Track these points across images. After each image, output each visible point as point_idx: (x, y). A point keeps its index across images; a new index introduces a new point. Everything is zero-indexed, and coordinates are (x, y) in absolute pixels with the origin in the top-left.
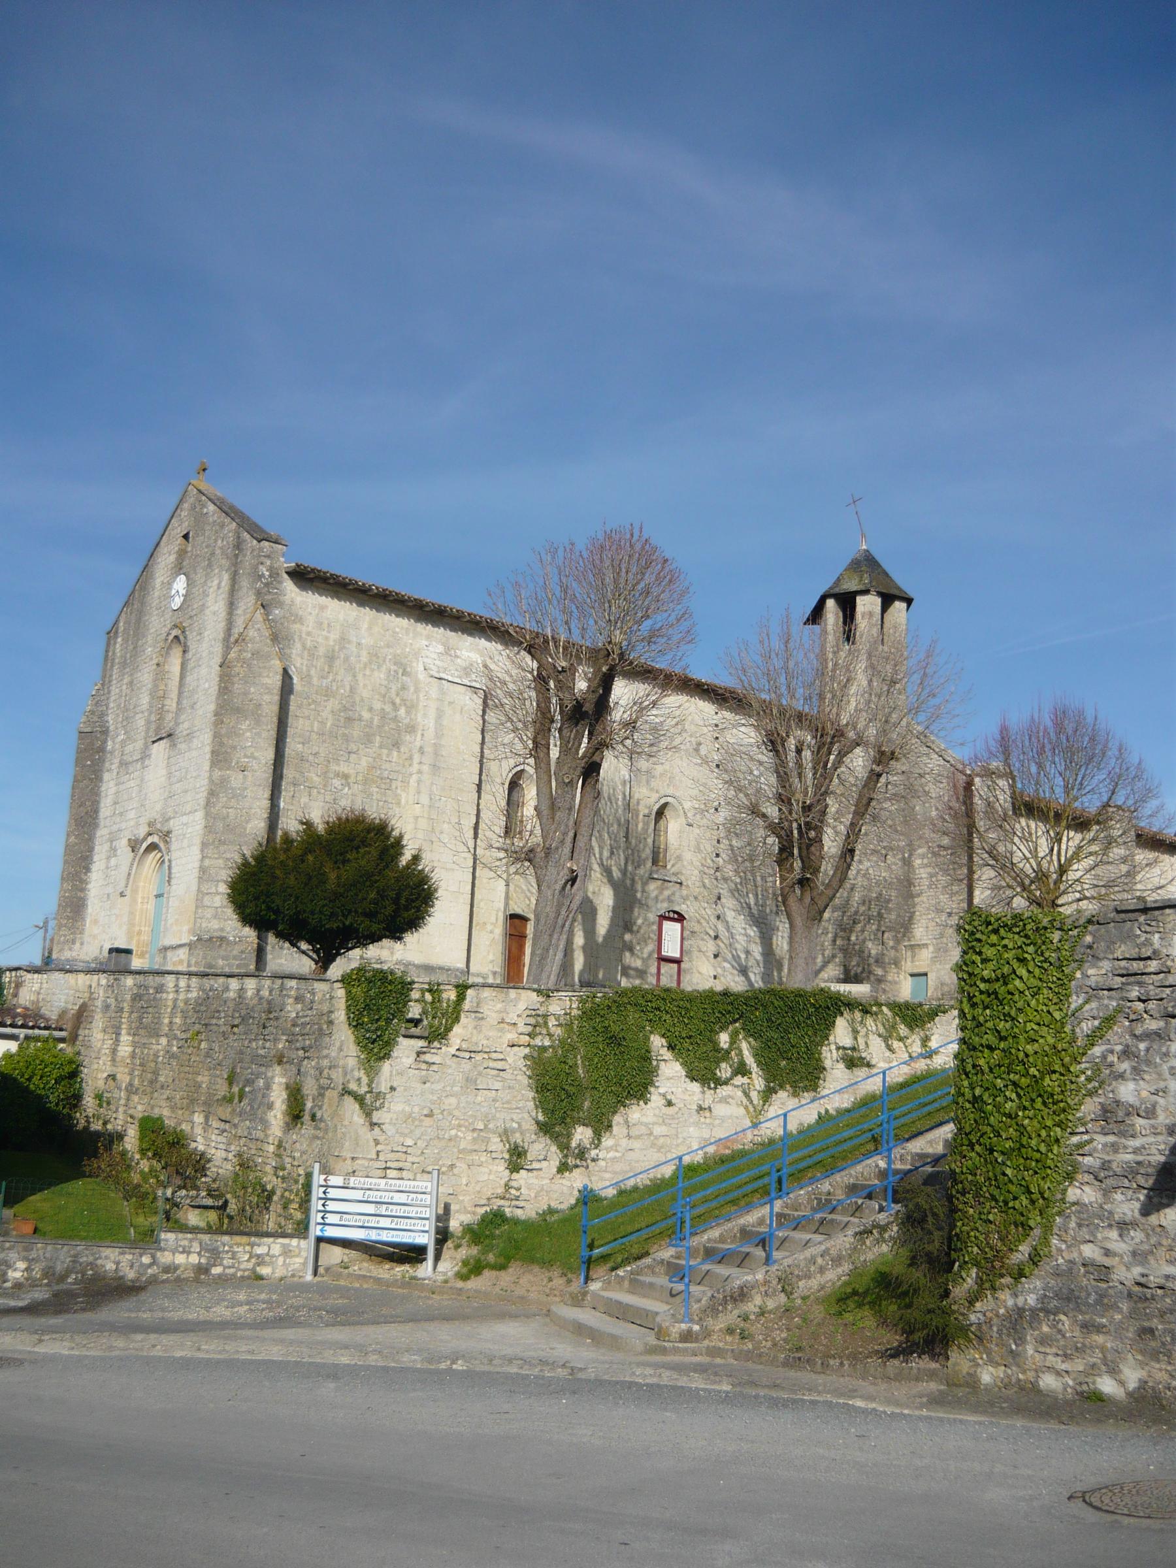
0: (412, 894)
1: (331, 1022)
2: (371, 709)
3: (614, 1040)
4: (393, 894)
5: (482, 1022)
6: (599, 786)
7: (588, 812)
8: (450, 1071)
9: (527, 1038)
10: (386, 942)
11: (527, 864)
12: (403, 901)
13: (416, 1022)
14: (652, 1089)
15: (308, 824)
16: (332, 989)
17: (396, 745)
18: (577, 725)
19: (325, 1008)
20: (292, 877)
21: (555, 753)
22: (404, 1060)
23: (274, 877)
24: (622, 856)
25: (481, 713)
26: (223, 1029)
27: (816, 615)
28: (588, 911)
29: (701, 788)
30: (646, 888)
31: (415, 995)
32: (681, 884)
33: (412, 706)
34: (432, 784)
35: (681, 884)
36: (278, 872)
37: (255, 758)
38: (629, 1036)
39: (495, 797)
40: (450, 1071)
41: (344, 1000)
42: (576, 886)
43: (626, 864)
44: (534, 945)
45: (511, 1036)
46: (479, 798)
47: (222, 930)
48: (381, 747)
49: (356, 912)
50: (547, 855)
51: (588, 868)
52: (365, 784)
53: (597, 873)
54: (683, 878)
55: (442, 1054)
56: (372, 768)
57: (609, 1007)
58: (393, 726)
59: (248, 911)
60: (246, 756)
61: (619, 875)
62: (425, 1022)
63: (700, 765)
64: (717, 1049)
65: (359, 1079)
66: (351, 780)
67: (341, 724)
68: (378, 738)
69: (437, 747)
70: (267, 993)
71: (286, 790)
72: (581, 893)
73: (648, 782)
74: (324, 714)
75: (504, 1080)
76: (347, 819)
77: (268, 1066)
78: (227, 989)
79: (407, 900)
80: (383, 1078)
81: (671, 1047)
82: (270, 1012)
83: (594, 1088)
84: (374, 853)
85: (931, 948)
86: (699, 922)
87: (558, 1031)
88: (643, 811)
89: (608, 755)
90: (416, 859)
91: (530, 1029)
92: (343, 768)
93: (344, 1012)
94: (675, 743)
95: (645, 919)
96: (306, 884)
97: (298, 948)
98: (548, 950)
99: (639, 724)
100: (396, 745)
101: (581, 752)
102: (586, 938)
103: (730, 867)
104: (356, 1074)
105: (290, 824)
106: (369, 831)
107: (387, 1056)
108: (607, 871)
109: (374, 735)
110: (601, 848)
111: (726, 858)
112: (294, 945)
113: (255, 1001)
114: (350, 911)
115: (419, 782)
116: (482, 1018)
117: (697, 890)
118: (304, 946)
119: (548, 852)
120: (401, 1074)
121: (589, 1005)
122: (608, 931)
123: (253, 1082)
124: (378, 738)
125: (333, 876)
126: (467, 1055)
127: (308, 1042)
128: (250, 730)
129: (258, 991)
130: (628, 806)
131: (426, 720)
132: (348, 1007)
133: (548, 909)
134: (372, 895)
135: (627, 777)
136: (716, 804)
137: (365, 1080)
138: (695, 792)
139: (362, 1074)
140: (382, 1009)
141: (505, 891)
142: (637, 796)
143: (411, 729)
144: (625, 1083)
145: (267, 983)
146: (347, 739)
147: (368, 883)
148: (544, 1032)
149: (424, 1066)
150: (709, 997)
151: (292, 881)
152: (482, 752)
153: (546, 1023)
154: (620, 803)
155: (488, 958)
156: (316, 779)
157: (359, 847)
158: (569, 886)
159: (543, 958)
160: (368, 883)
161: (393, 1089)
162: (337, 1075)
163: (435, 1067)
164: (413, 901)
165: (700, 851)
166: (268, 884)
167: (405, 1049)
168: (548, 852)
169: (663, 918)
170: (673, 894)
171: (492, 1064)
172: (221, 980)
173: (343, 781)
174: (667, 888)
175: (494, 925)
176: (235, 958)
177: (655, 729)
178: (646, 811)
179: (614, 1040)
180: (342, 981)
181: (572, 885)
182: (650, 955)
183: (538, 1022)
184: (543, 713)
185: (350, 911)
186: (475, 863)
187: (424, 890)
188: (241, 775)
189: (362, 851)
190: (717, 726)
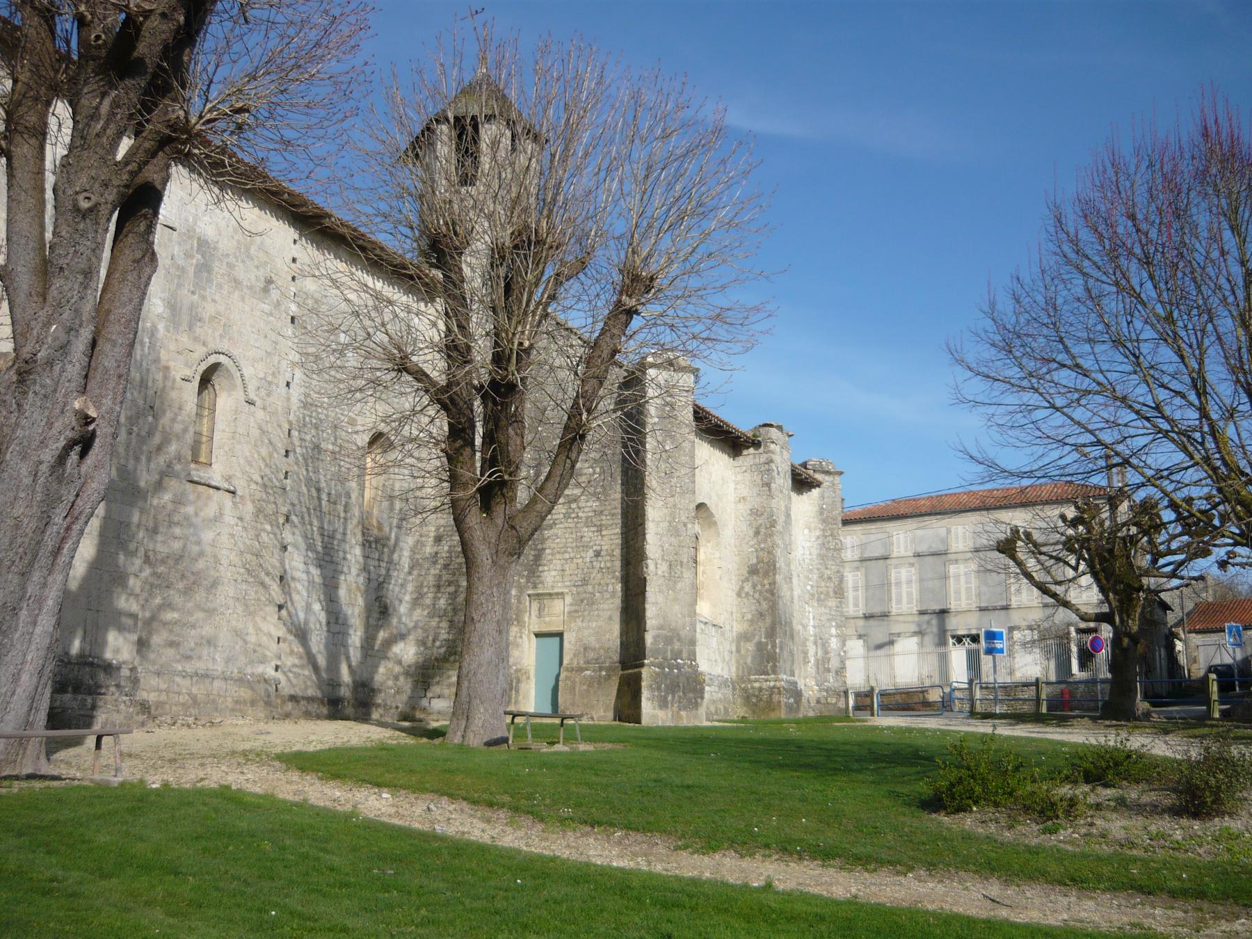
21: (55, 151)
27: (422, 142)
32: (233, 493)
85: (568, 599)
133: (19, 510)
158: (74, 456)
166: (790, 708)
181: (83, 455)
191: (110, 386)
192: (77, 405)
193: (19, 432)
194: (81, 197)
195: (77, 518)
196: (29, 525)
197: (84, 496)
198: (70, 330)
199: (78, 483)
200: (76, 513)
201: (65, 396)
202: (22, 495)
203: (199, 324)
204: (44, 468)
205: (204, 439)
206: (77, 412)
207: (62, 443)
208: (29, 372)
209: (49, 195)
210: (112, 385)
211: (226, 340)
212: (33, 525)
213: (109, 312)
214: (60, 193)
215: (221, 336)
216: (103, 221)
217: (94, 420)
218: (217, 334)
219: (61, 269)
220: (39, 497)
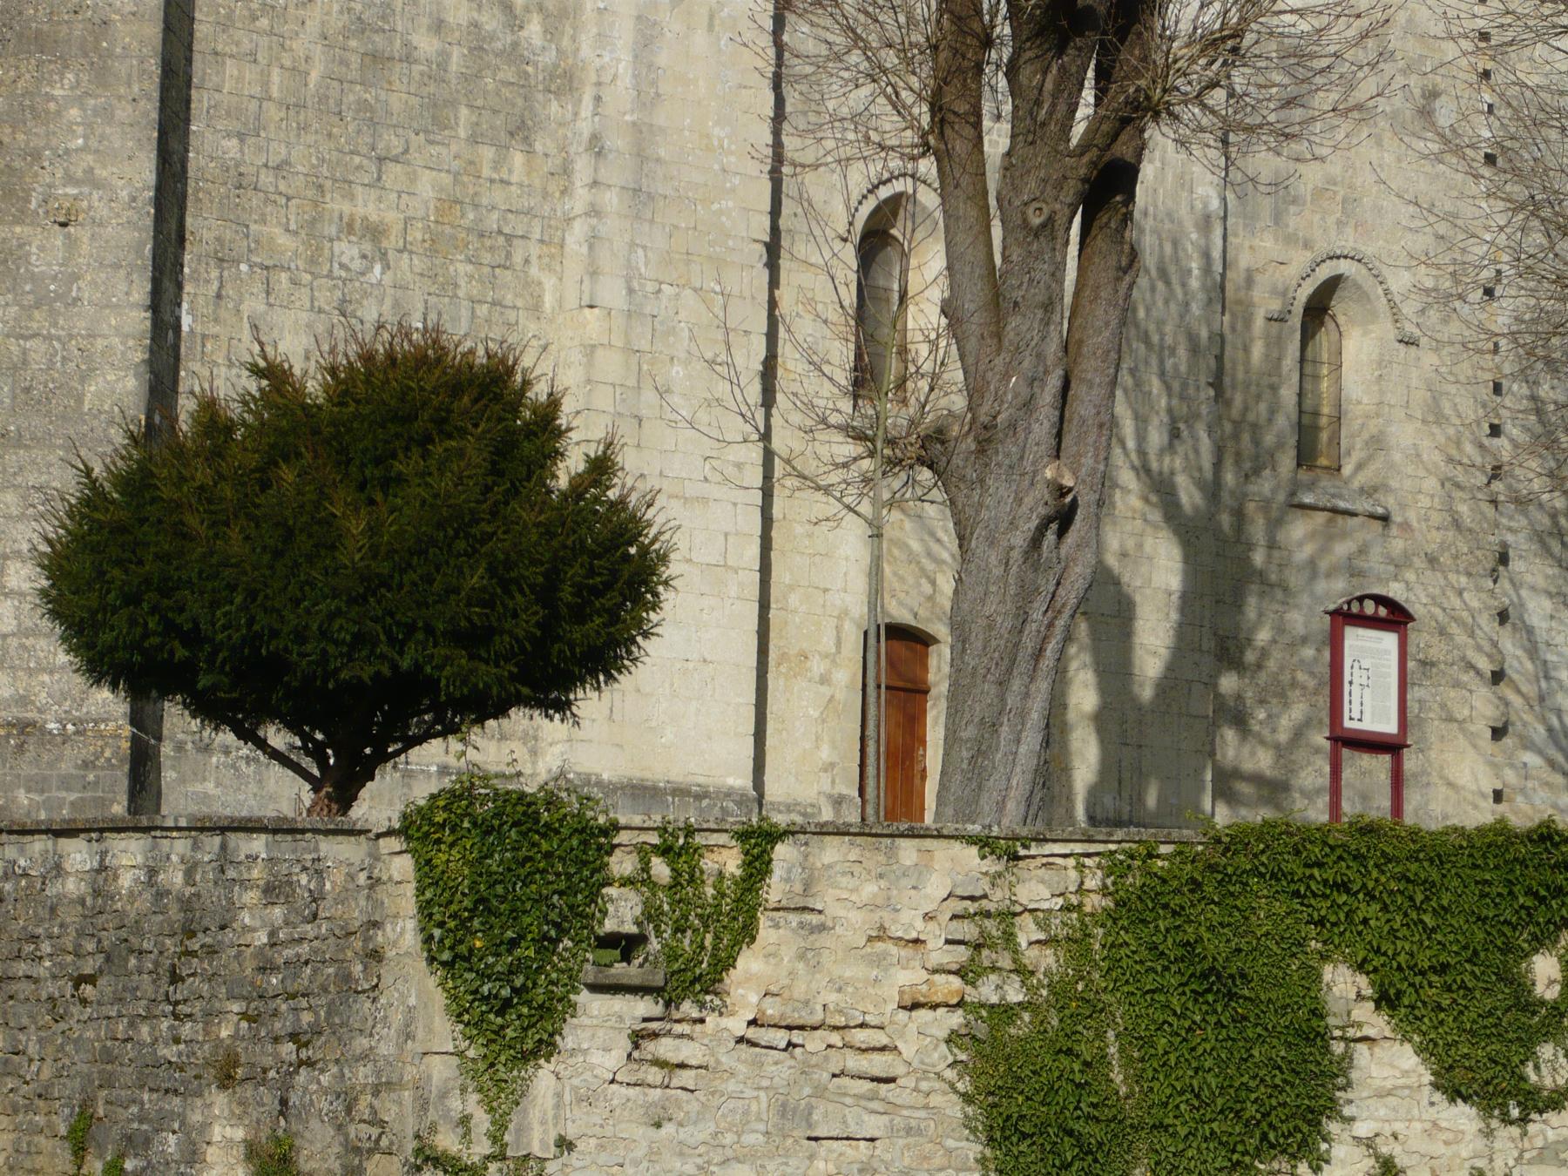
0: (592, 572)
1: (375, 955)
2: (439, 26)
3: (1214, 983)
4: (535, 574)
5: (823, 940)
6: (1131, 234)
7: (1102, 315)
8: (732, 1086)
9: (956, 982)
10: (519, 718)
11: (925, 475)
12: (566, 594)
13: (626, 945)
14: (1333, 1127)
15: (273, 374)
16: (376, 857)
17: (521, 131)
18: (1061, 51)
19: (356, 913)
20: (234, 533)
21: (997, 139)
22: (596, 1058)
23: (182, 534)
24: (1206, 444)
25: (769, 24)
26: (51, 988)
28: (1110, 612)
29: (1442, 228)
30: (1281, 536)
31: (622, 864)
32: (1385, 519)
33: (563, 14)
34: (633, 245)
35: (1385, 519)
36: (192, 520)
37: (97, 184)
38: (1260, 967)
39: (822, 280)
40: (732, 1086)
41: (410, 889)
42: (1072, 537)
43: (1218, 465)
44: (953, 713)
45: (908, 977)
46: (774, 283)
47: (23, 701)
48: (474, 140)
49: (429, 630)
50: (984, 446)
51: (1105, 484)
52: (433, 252)
53: (1130, 496)
54: (1391, 502)
55: (710, 1036)
56: (450, 203)
57: (1196, 885)
58: (508, 74)
59: (106, 638)
60: (70, 179)
61: (1198, 498)
62: (654, 945)
63: (1438, 158)
64: (1524, 1001)
65: (465, 1121)
66: (392, 242)
67: (354, 75)
68: (464, 112)
69: (642, 134)
70: (178, 878)
71: (196, 280)
72: (1089, 557)
73: (1278, 218)
74: (299, 46)
75: (892, 1107)
76: (391, 357)
77: (189, 1092)
78: (58, 870)
79: (579, 589)
80: (534, 1115)
81: (1385, 1000)
82: (192, 934)
83: (1160, 1127)
84: (475, 452)
86: (1442, 632)
87: (1045, 960)
88: (1265, 303)
89: (1160, 141)
90: (601, 468)
91: (962, 954)
92: (366, 206)
93: (411, 925)
94: (1360, 95)
95: (1280, 629)
96: (278, 554)
97: (262, 744)
98: (995, 727)
99: (1249, 38)
100: (521, 131)
101: (1078, 130)
102: (1103, 689)
103: (1534, 464)
104: (455, 1104)
105: (219, 375)
106: (456, 390)
107: (547, 1047)
108: (1161, 489)
109: (453, 103)
110: (1141, 421)
111: (1523, 438)
112: (248, 735)
113: (145, 902)
114: (411, 629)
115: (593, 240)
116: (822, 928)
117: (1437, 536)
118: (278, 737)
119: (986, 436)
120: (587, 1099)
121: (1134, 880)
122: (1171, 668)
123: (147, 1142)
124: (464, 112)
125: (356, 526)
126: (780, 1038)
127: (306, 1018)
128: (80, 101)
129: (152, 872)
130: (1218, 292)
131: (608, 56)
132: (425, 910)
133: (990, 608)
134: (476, 579)
135: (1215, 204)
136: (1488, 274)
137: (482, 1121)
138: (1422, 242)
139: (472, 1103)
140: (533, 917)
141: (839, 573)
142: (1244, 260)
143: (564, 82)
144: (1251, 1110)
145: (179, 847)
146: (372, 118)
147: (461, 545)
148: (1005, 962)
149: (654, 1075)
150: (1496, 845)
151: (235, 543)
152: (777, 145)
153: (1009, 937)
154: (1194, 283)
155: (816, 760)
156: (283, 240)
157: (428, 439)
158: (1050, 537)
159: (981, 752)
160: (461, 545)
161: (564, 1144)
162: (399, 1112)
163: (686, 1078)
164: (598, 592)
165: (1440, 419)
167: (599, 1026)
168: (986, 436)
169: (1344, 617)
170: (1363, 551)
171: (854, 1062)
172: (39, 845)
173: (367, 247)
174: (1344, 535)
175: (832, 659)
176: (66, 783)
177: (1297, 56)
178: (1275, 306)
179: (1214, 983)
180: (404, 832)
181: (1061, 533)
182: (1298, 734)
183: (986, 932)
184: (957, 19)
185: (411, 629)
186: (768, 476)
187: (627, 558)
188: (58, 238)
189: (438, 449)
190: (1484, 36)
191: (1091, 440)
192: (1049, 474)
193: (984, 514)
194: (1030, 211)
195: (1060, 612)
196: (1005, 624)
197: (1066, 583)
198: (1031, 382)
199: (1058, 569)
200: (1058, 605)
201: (1034, 463)
202: (993, 589)
203: (1292, 209)
204: (1016, 555)
205: (1324, 421)
206: (1049, 483)
207: (1034, 523)
208: (989, 441)
209: (993, 202)
210: (1091, 439)
211: (1349, 230)
212: (1008, 624)
213: (1080, 342)
214: (1006, 203)
215: (1339, 223)
216: (1060, 233)
217: (1070, 490)
218: (1331, 220)
219: (1016, 304)
220: (1012, 590)
